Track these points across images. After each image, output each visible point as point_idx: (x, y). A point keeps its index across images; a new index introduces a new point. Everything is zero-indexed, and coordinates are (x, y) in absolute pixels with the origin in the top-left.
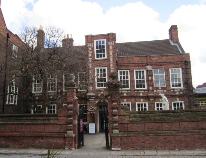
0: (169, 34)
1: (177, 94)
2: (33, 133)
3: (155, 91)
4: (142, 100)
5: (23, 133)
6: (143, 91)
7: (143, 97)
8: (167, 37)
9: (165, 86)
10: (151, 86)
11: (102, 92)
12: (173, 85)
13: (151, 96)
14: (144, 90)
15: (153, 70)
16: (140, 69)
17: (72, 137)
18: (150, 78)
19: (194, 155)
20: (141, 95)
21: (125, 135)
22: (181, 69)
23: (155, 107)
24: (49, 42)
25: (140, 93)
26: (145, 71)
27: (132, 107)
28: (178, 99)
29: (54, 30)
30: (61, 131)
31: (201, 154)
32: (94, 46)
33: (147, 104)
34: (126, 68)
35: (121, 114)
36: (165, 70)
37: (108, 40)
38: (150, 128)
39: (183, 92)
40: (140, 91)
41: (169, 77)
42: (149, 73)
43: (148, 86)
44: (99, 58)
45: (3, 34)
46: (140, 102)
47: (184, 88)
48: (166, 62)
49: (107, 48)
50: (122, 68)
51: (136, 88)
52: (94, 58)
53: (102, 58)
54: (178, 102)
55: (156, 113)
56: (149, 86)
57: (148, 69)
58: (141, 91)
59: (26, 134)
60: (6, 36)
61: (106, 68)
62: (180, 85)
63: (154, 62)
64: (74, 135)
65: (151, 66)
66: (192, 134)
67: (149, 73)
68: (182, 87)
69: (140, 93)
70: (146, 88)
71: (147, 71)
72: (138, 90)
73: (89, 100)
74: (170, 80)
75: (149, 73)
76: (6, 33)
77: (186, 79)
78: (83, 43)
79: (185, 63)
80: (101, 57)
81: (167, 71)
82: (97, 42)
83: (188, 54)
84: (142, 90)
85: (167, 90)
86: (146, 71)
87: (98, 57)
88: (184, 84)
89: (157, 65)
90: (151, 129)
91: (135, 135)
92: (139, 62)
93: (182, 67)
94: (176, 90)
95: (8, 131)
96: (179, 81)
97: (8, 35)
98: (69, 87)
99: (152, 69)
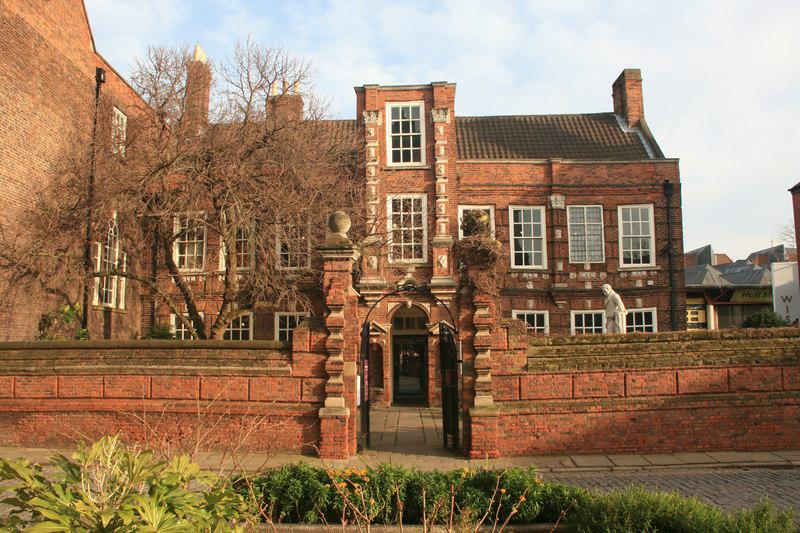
0: (614, 95)
1: (639, 284)
2: (613, 414)
3: (573, 275)
4: (639, 301)
5: (175, 402)
6: (536, 275)
7: (534, 294)
8: (608, 106)
9: (604, 261)
10: (560, 259)
11: (409, 276)
12: (627, 257)
13: (560, 291)
14: (540, 272)
15: (568, 207)
16: (527, 204)
17: (342, 419)
18: (558, 233)
19: (720, 465)
20: (530, 286)
21: (513, 411)
22: (651, 208)
23: (569, 326)
24: (249, 103)
25: (526, 281)
26: (543, 209)
27: (659, 323)
28: (531, 303)
29: (270, 64)
30: (304, 399)
31: (740, 464)
32: (384, 124)
33: (546, 314)
34: (486, 199)
35: (501, 346)
36: (604, 210)
37: (430, 103)
38: (589, 389)
39: (655, 279)
40: (525, 275)
41: (617, 233)
42: (555, 218)
43: (552, 259)
44: (402, 164)
45: (85, 70)
46: (528, 309)
47: (659, 268)
48: (610, 186)
49: (426, 131)
50: (473, 200)
51: (513, 266)
52: (385, 164)
53: (412, 164)
54: (291, 314)
55: (608, 343)
56: (553, 259)
57: (554, 206)
58: (530, 275)
59: (184, 406)
60: (93, 76)
61: (424, 198)
62: (646, 259)
63: (573, 182)
64: (348, 412)
65: (563, 198)
66: (713, 404)
67: (556, 219)
68: (653, 263)
69: (526, 281)
70: (545, 266)
71: (550, 212)
72: (522, 271)
73: (367, 301)
74: (617, 242)
75: (556, 219)
76: (94, 65)
77: (665, 240)
78: (344, 108)
79: (666, 192)
80: (407, 159)
81: (610, 213)
82: (395, 111)
83: (675, 162)
84: (532, 271)
85: (608, 274)
86: (547, 211)
87: (396, 158)
88: (658, 256)
89: (580, 192)
90: (592, 392)
91: (541, 409)
92: (527, 183)
93: (655, 203)
94: (634, 273)
95: (126, 394)
96: (646, 245)
97: (99, 72)
98: (333, 253)
99: (566, 204)
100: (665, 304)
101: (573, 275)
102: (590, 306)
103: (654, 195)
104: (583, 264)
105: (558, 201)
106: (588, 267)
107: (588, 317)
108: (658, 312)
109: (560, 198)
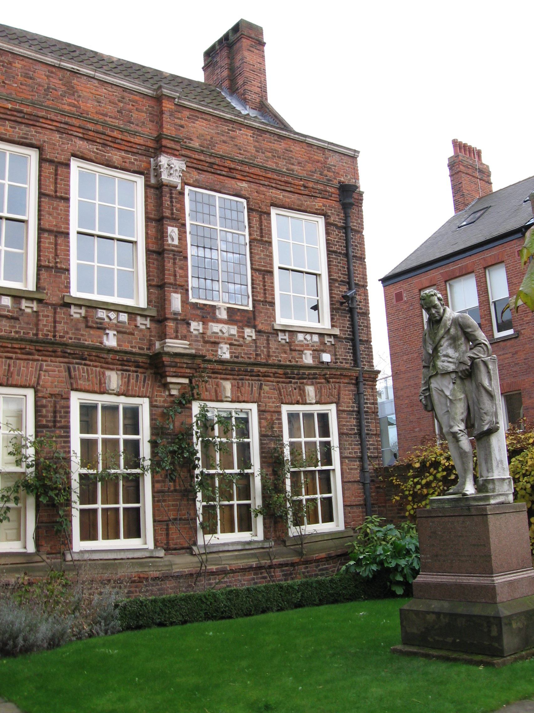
1: (308, 359)
3: (196, 326)
6: (124, 317)
7: (121, 359)
9: (250, 308)
14: (132, 313)
18: (172, 231)
25: (101, 327)
27: (341, 434)
33: (144, 406)
36: (250, 210)
40: (102, 314)
42: (167, 203)
58: (113, 315)
69: (101, 327)
85: (259, 332)
86: (147, 186)
100: (348, 402)
101: (196, 326)
102: (229, 394)
103: (328, 202)
104: (214, 307)
105: (172, 168)
106: (223, 315)
107: (111, 410)
108: (339, 411)
109: (179, 164)
